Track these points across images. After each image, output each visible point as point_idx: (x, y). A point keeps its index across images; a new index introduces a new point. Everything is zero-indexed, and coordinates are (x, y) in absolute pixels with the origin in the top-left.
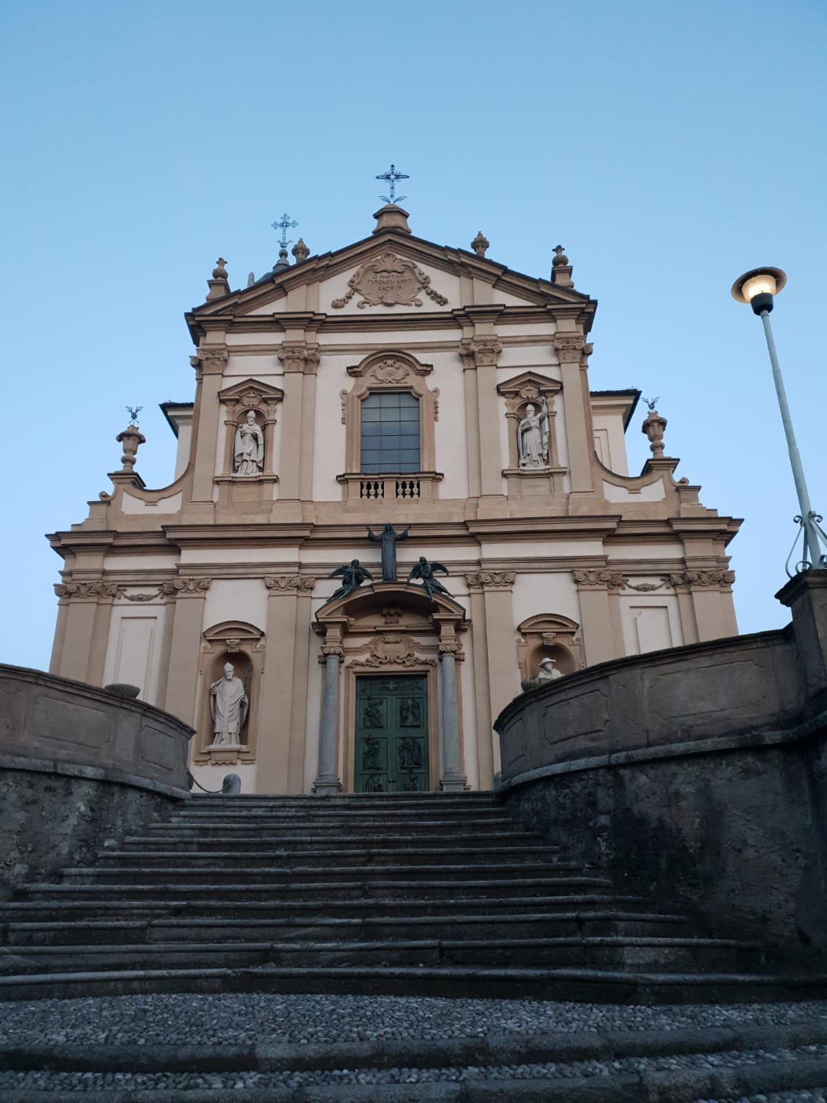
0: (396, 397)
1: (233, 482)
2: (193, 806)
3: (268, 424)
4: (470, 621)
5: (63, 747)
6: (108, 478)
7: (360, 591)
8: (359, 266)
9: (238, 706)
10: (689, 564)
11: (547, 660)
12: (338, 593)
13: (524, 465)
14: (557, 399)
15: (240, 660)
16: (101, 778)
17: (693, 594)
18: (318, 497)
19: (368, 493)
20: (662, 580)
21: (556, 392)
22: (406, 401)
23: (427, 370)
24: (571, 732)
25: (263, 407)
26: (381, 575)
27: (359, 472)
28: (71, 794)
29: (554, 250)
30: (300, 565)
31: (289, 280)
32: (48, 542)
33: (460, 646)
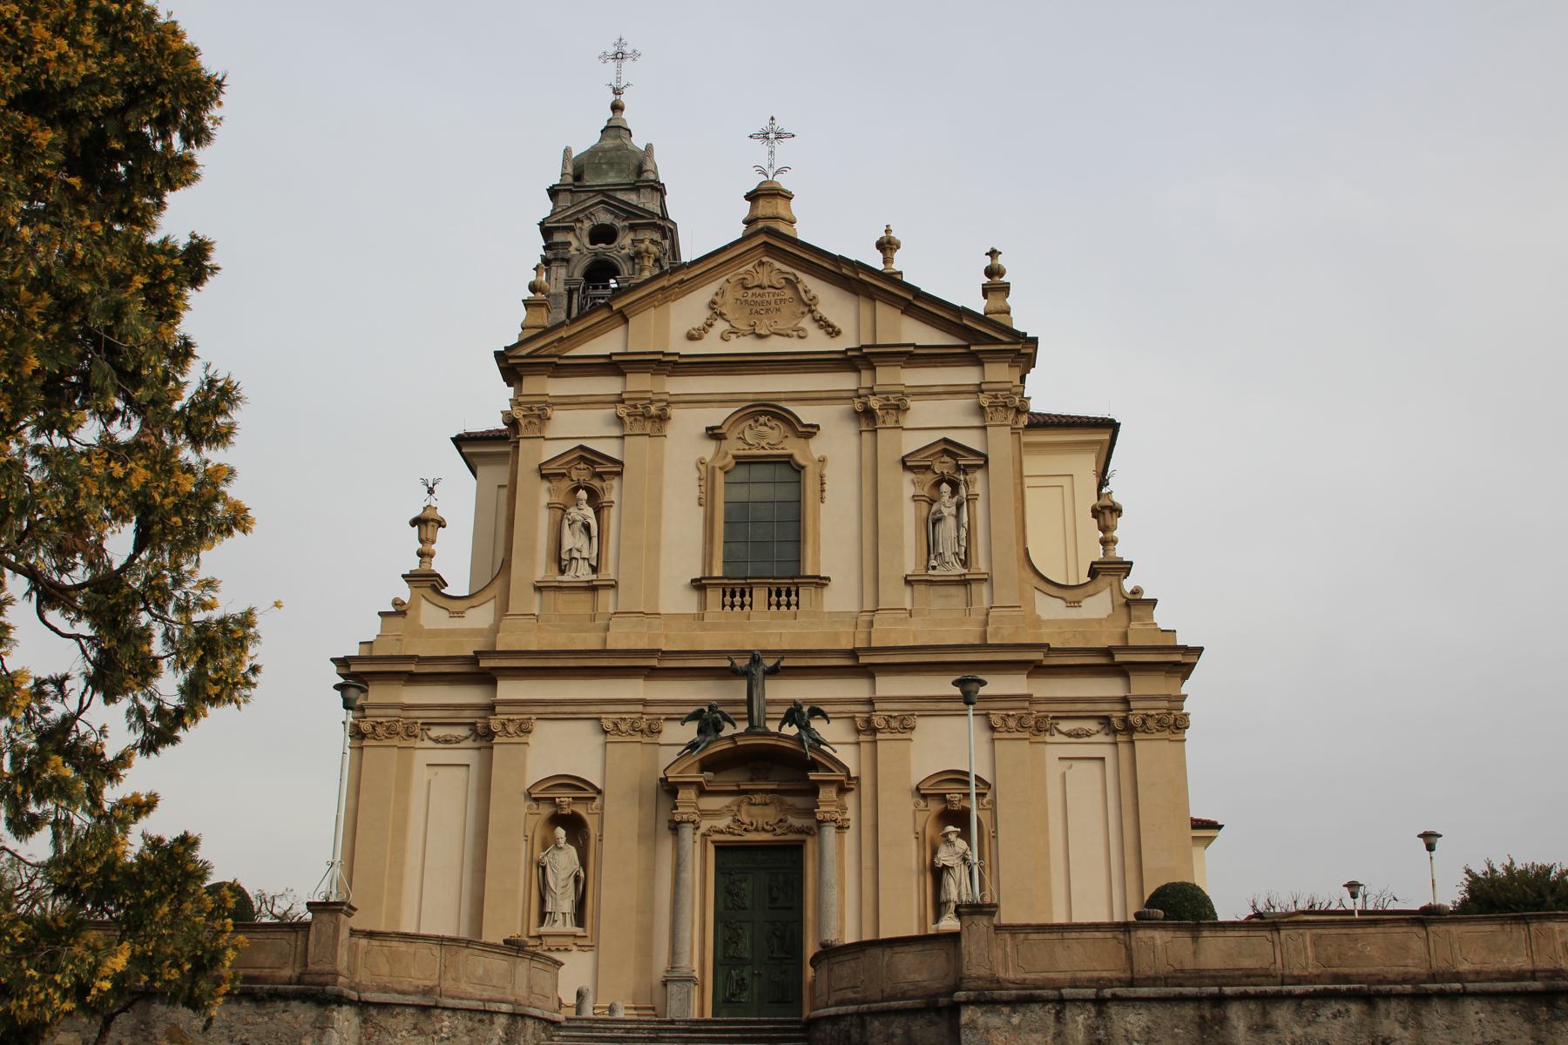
0: (771, 467)
1: (559, 588)
2: (567, 1027)
3: (603, 507)
4: (858, 778)
5: (484, 990)
6: (403, 580)
7: (719, 743)
8: (724, 279)
9: (572, 880)
10: (1133, 705)
11: (951, 828)
12: (693, 746)
13: (934, 568)
14: (979, 475)
15: (575, 827)
16: (511, 1012)
17: (1136, 742)
18: (666, 607)
19: (733, 602)
20: (1101, 724)
21: (978, 467)
22: (782, 473)
23: (810, 432)
24: (844, 985)
25: (596, 483)
26: (746, 716)
27: (721, 575)
28: (494, 1023)
29: (987, 254)
30: (645, 703)
31: (628, 304)
32: (333, 667)
33: (844, 809)
